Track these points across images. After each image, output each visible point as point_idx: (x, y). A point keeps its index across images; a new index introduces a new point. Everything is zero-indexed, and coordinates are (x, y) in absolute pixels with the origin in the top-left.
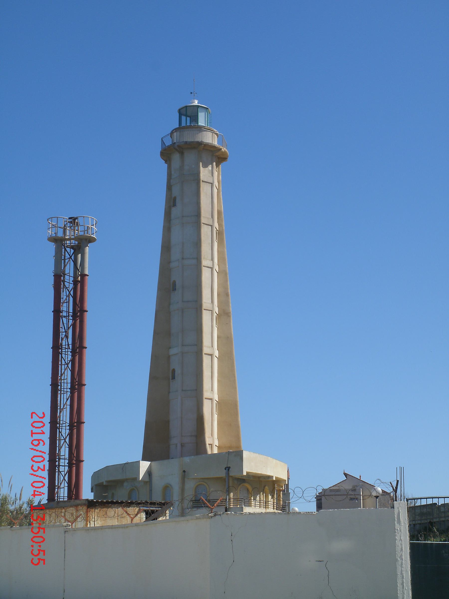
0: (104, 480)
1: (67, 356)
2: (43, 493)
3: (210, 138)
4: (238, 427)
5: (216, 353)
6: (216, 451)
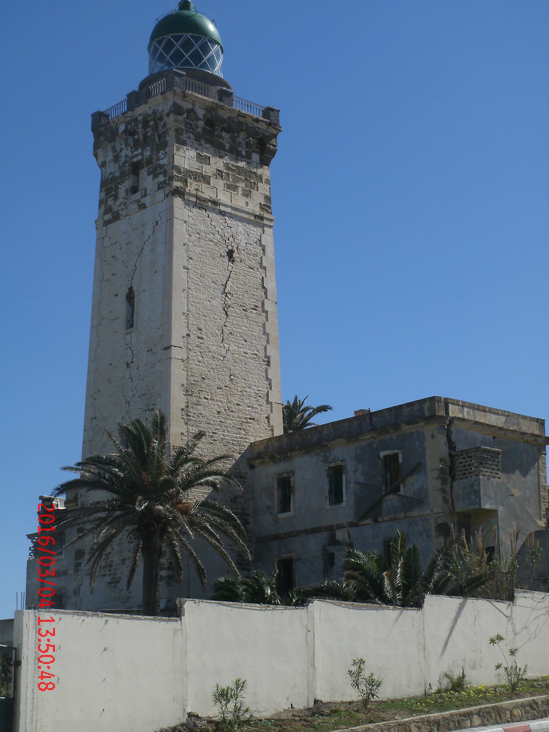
2: (52, 675)
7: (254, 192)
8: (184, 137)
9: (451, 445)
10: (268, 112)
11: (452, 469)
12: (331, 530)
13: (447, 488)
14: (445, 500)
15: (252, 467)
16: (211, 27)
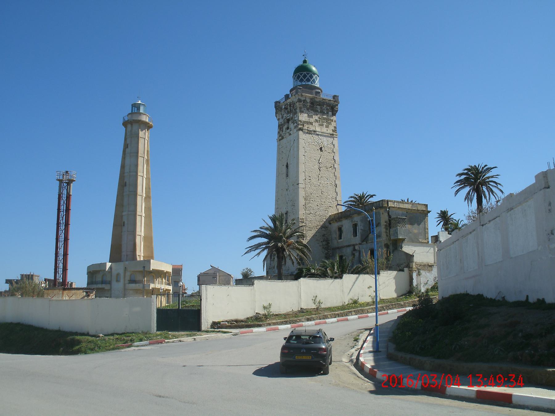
0: (91, 270)
1: (62, 227)
3: (145, 118)
4: (152, 248)
5: (144, 215)
6: (142, 259)
7: (330, 126)
8: (303, 110)
9: (389, 216)
10: (335, 97)
11: (390, 224)
12: (354, 245)
13: (388, 231)
14: (387, 236)
15: (330, 224)
16: (314, 69)
